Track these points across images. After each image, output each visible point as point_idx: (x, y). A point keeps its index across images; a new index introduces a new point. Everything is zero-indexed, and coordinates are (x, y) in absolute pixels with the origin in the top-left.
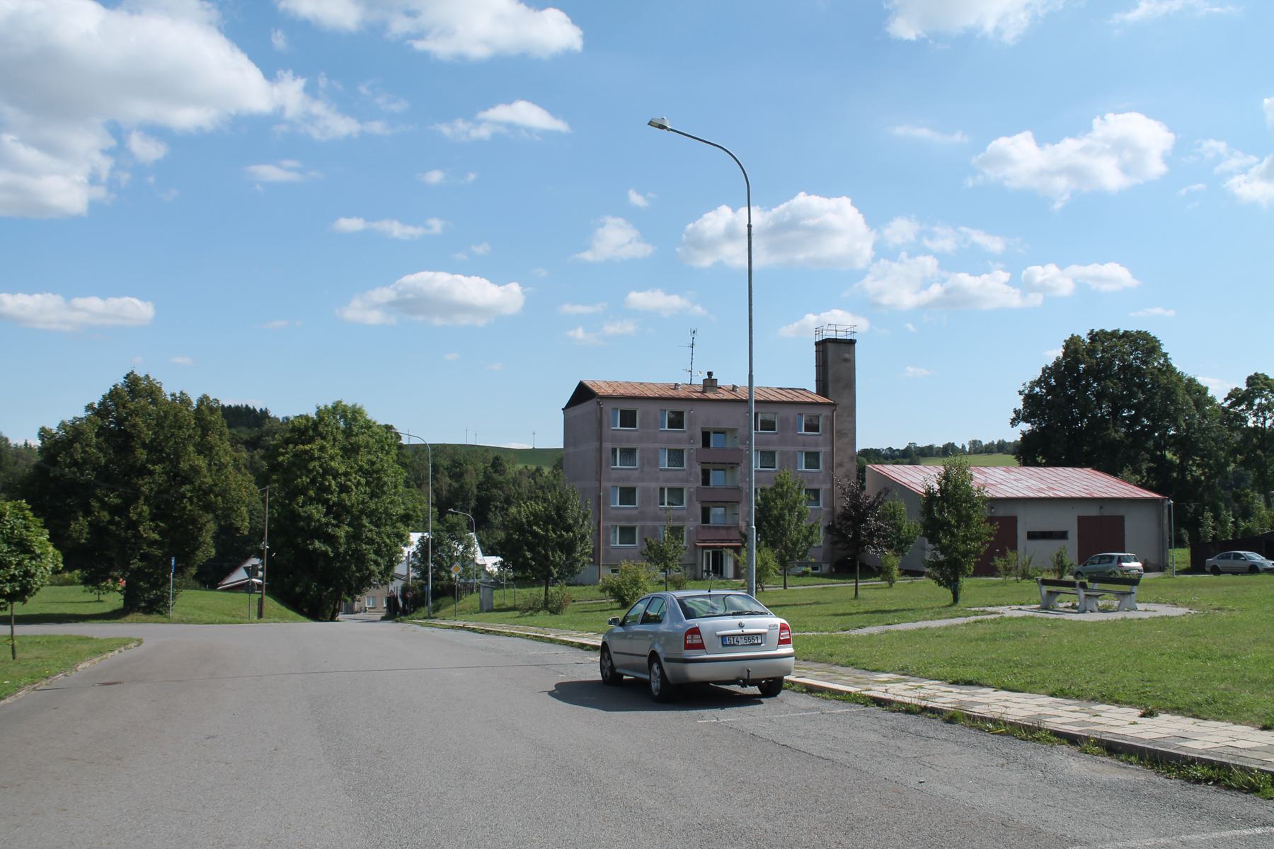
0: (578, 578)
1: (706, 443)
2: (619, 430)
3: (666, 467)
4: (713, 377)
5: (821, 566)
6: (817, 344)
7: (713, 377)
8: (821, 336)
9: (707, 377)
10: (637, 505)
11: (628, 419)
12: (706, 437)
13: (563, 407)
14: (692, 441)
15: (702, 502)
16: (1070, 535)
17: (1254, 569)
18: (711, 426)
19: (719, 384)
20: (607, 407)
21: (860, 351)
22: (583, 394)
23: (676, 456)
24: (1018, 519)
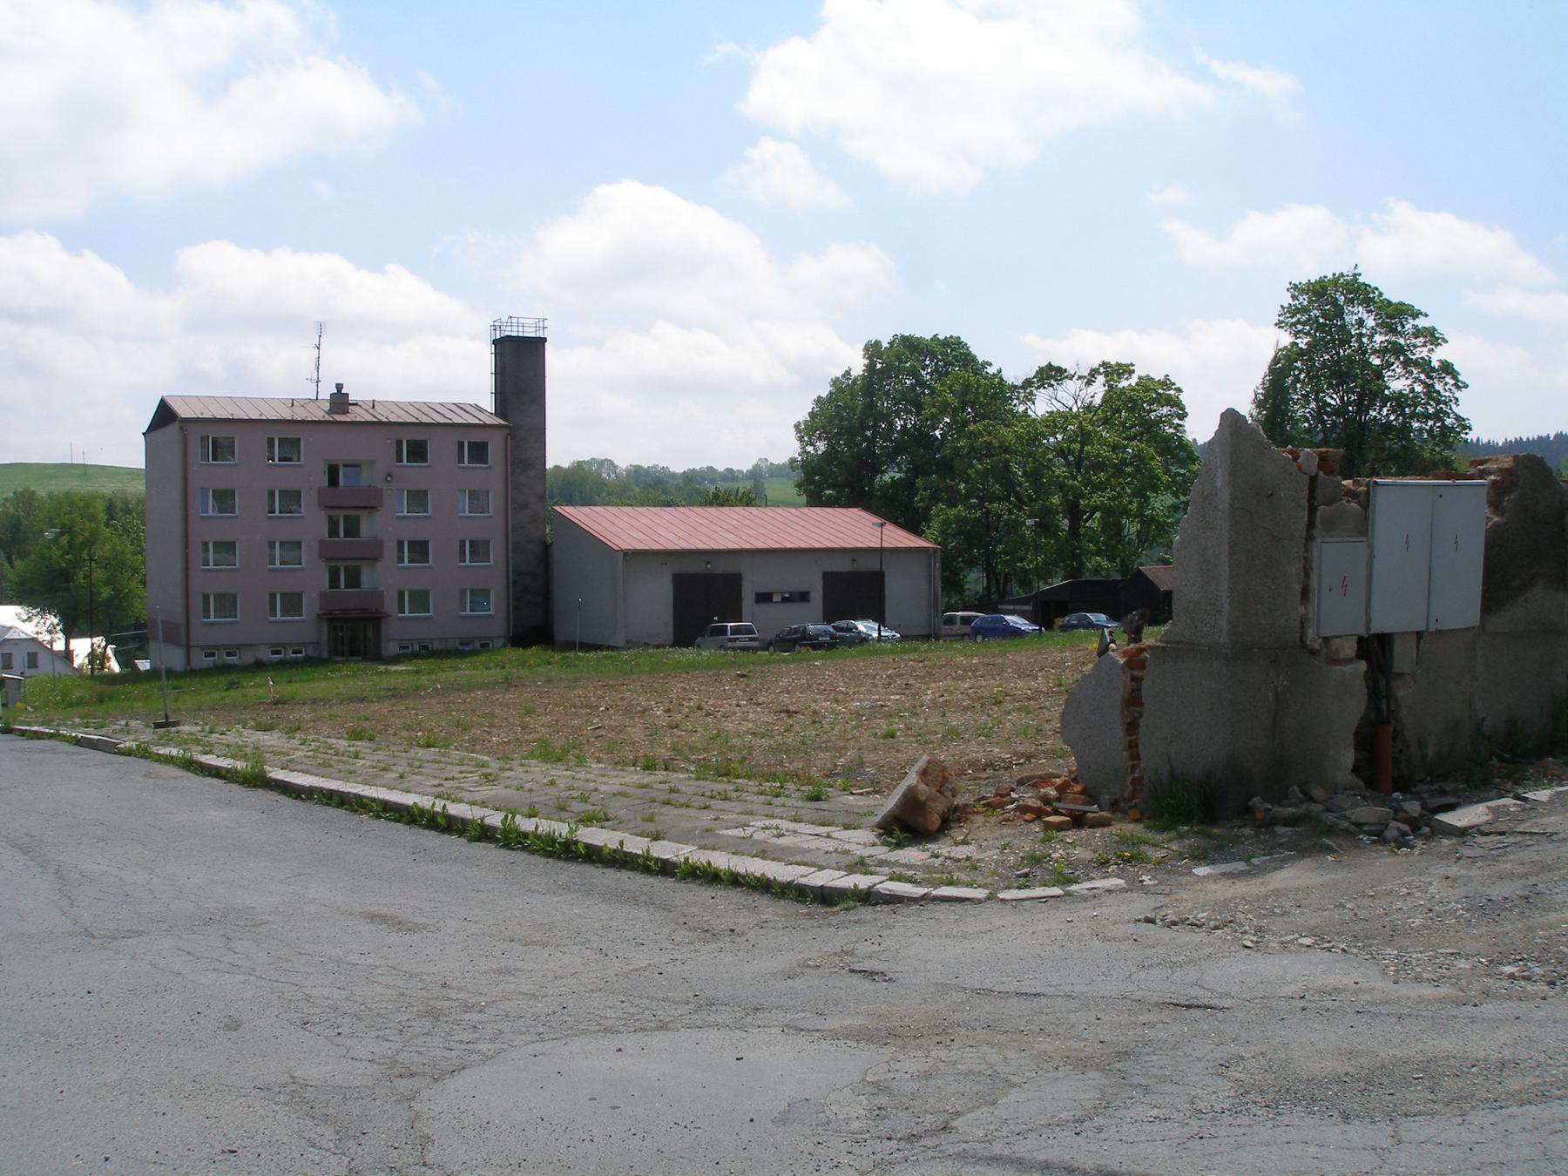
0: (1356, 638)
1: (333, 479)
2: (406, 466)
3: (405, 513)
4: (343, 391)
5: (412, 644)
6: (495, 342)
7: (343, 391)
8: (498, 332)
9: (336, 391)
10: (491, 563)
11: (418, 451)
12: (333, 472)
13: (144, 431)
14: (389, 478)
15: (327, 559)
16: (812, 595)
17: (1016, 633)
18: (338, 456)
19: (352, 398)
20: (195, 434)
21: (549, 349)
22: (164, 415)
23: (477, 498)
24: (743, 576)
